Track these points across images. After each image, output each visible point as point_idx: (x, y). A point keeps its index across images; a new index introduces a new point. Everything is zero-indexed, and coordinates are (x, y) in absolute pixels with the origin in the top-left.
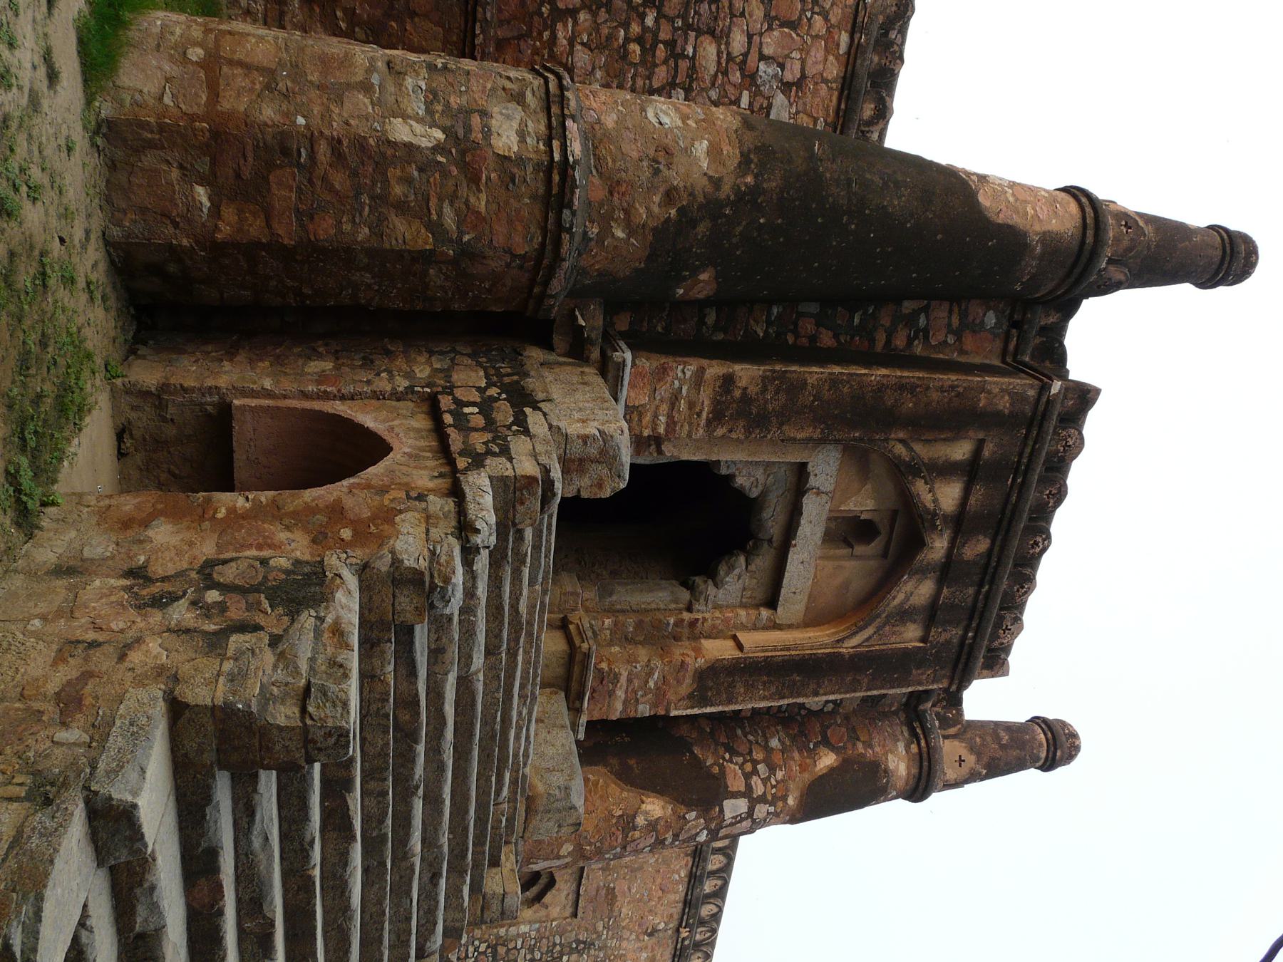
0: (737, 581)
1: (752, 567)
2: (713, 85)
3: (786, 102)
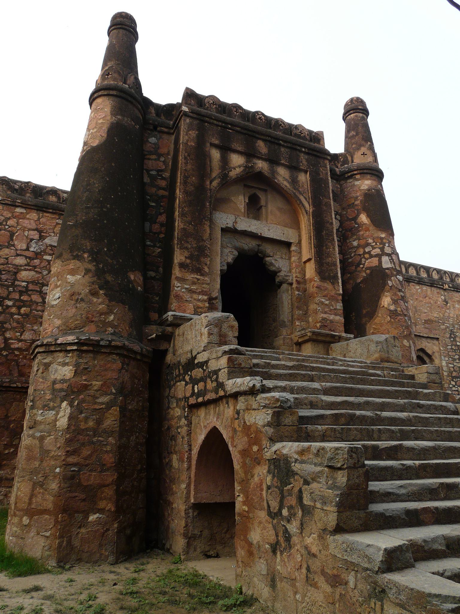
0: (278, 261)
1: (271, 254)
2: (40, 273)
3: (49, 238)
